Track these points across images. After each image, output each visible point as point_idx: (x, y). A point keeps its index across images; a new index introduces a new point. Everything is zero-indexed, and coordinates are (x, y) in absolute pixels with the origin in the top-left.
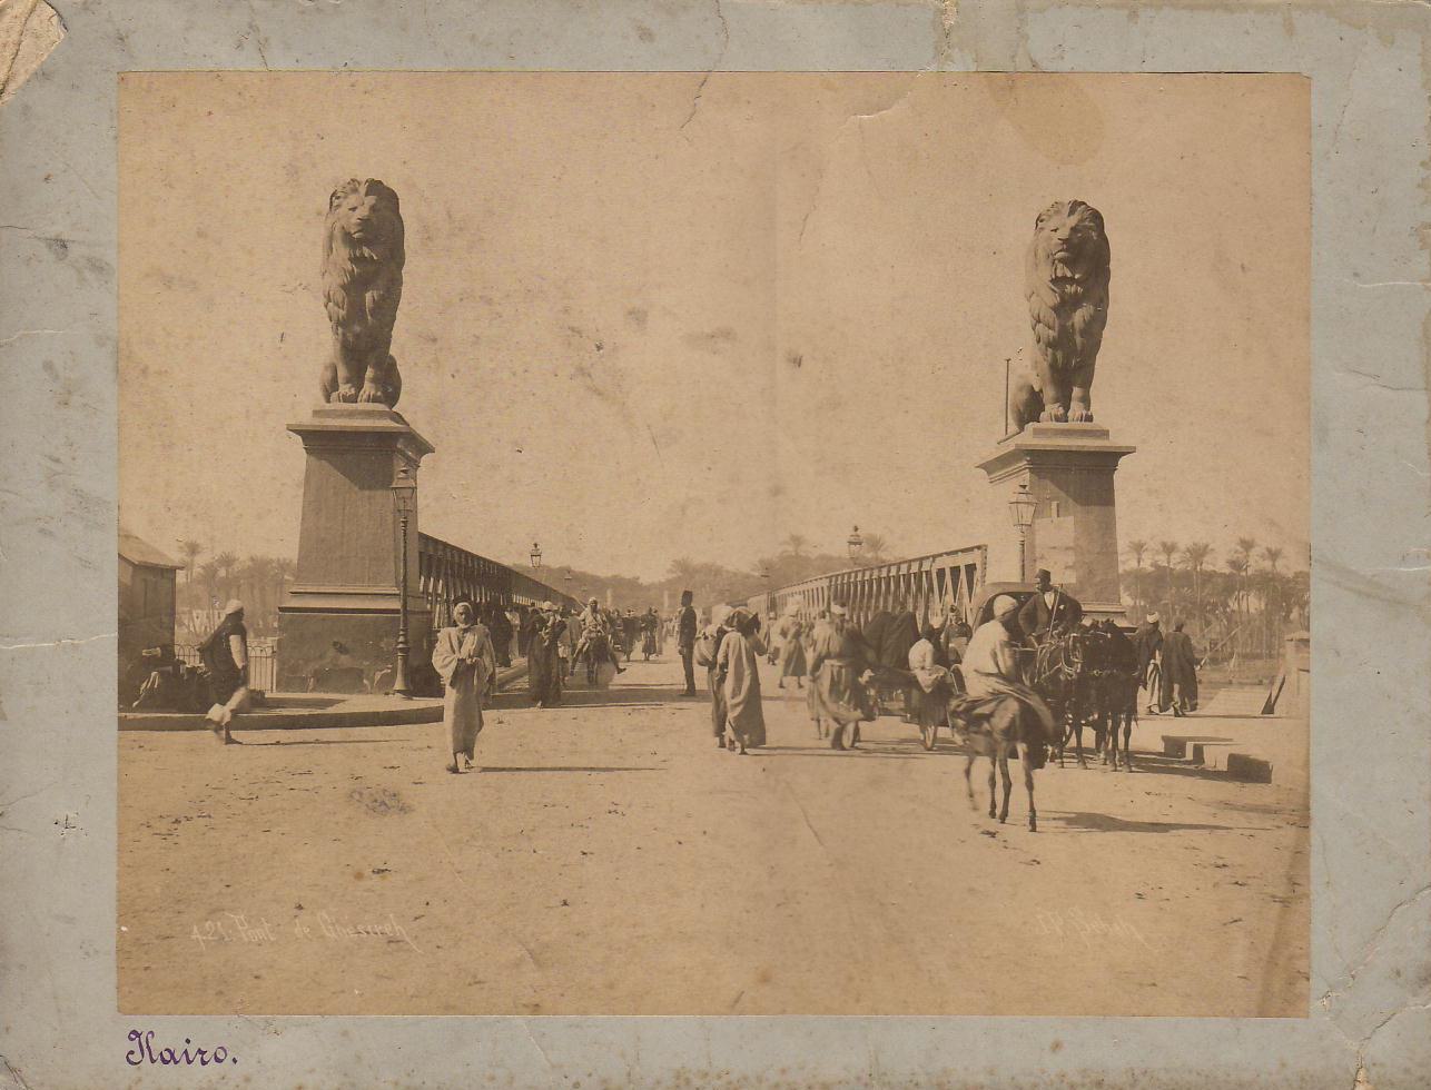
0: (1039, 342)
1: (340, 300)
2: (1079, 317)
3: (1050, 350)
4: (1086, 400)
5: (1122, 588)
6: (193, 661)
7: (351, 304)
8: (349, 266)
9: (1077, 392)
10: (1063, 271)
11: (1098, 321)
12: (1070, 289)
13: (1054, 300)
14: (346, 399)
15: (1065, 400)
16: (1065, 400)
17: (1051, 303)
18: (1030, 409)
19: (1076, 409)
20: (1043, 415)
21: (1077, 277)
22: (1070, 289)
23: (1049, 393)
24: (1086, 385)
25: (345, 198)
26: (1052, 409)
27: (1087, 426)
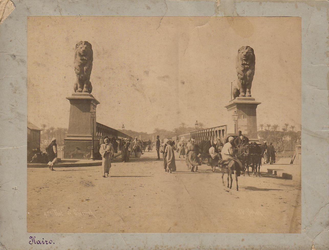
0: (239, 78)
1: (78, 69)
2: (248, 73)
3: (241, 80)
4: (250, 92)
5: (258, 135)
6: (44, 152)
7: (81, 70)
8: (80, 61)
9: (248, 90)
10: (244, 62)
11: (252, 74)
12: (246, 66)
13: (242, 69)
14: (80, 92)
15: (245, 92)
16: (245, 92)
17: (242, 70)
18: (237, 94)
19: (247, 94)
20: (240, 95)
21: (248, 63)
22: (246, 66)
23: (241, 90)
24: (250, 88)
25: (79, 45)
26: (242, 94)
27: (250, 98)
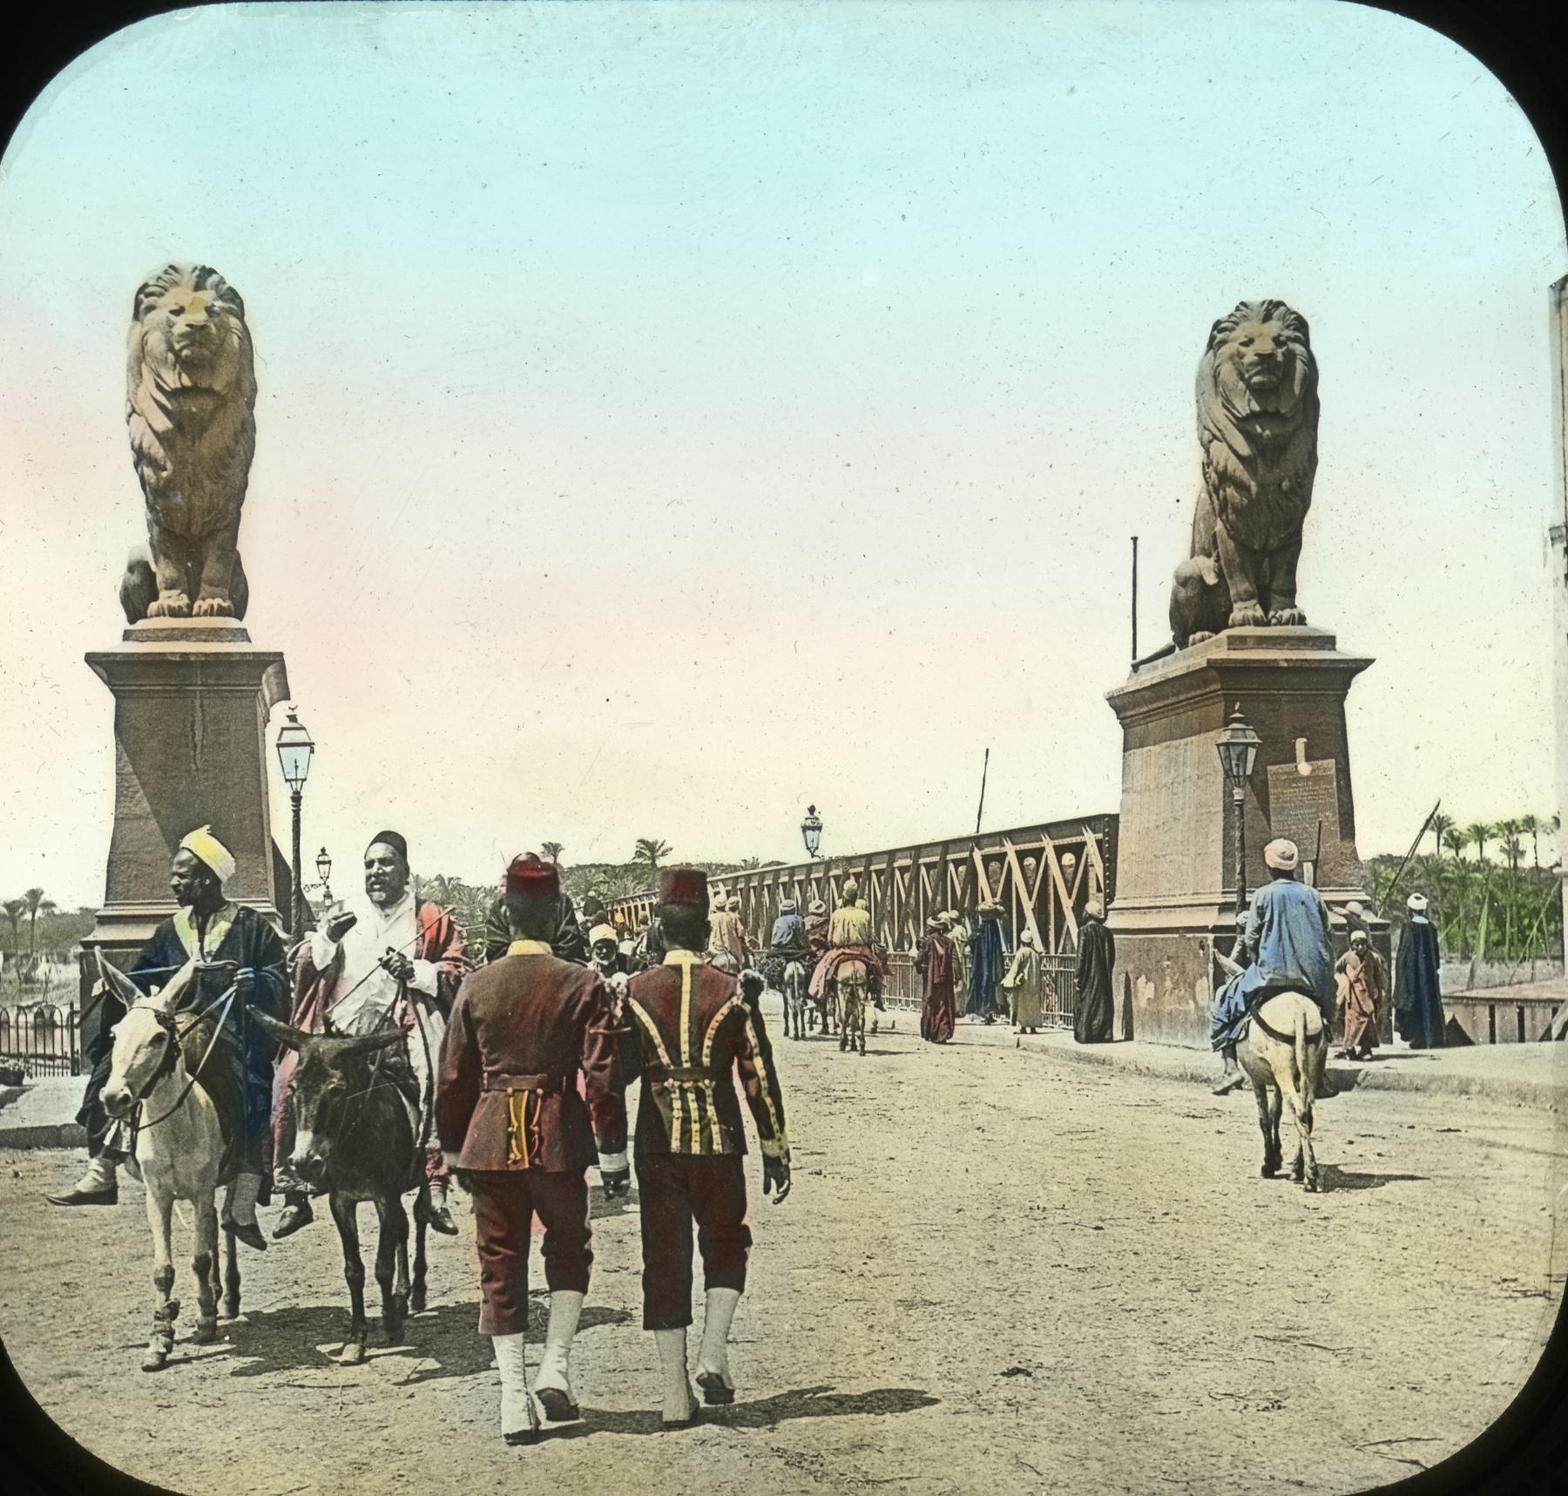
14: (175, 613)
